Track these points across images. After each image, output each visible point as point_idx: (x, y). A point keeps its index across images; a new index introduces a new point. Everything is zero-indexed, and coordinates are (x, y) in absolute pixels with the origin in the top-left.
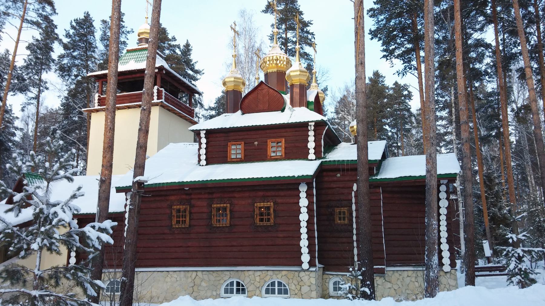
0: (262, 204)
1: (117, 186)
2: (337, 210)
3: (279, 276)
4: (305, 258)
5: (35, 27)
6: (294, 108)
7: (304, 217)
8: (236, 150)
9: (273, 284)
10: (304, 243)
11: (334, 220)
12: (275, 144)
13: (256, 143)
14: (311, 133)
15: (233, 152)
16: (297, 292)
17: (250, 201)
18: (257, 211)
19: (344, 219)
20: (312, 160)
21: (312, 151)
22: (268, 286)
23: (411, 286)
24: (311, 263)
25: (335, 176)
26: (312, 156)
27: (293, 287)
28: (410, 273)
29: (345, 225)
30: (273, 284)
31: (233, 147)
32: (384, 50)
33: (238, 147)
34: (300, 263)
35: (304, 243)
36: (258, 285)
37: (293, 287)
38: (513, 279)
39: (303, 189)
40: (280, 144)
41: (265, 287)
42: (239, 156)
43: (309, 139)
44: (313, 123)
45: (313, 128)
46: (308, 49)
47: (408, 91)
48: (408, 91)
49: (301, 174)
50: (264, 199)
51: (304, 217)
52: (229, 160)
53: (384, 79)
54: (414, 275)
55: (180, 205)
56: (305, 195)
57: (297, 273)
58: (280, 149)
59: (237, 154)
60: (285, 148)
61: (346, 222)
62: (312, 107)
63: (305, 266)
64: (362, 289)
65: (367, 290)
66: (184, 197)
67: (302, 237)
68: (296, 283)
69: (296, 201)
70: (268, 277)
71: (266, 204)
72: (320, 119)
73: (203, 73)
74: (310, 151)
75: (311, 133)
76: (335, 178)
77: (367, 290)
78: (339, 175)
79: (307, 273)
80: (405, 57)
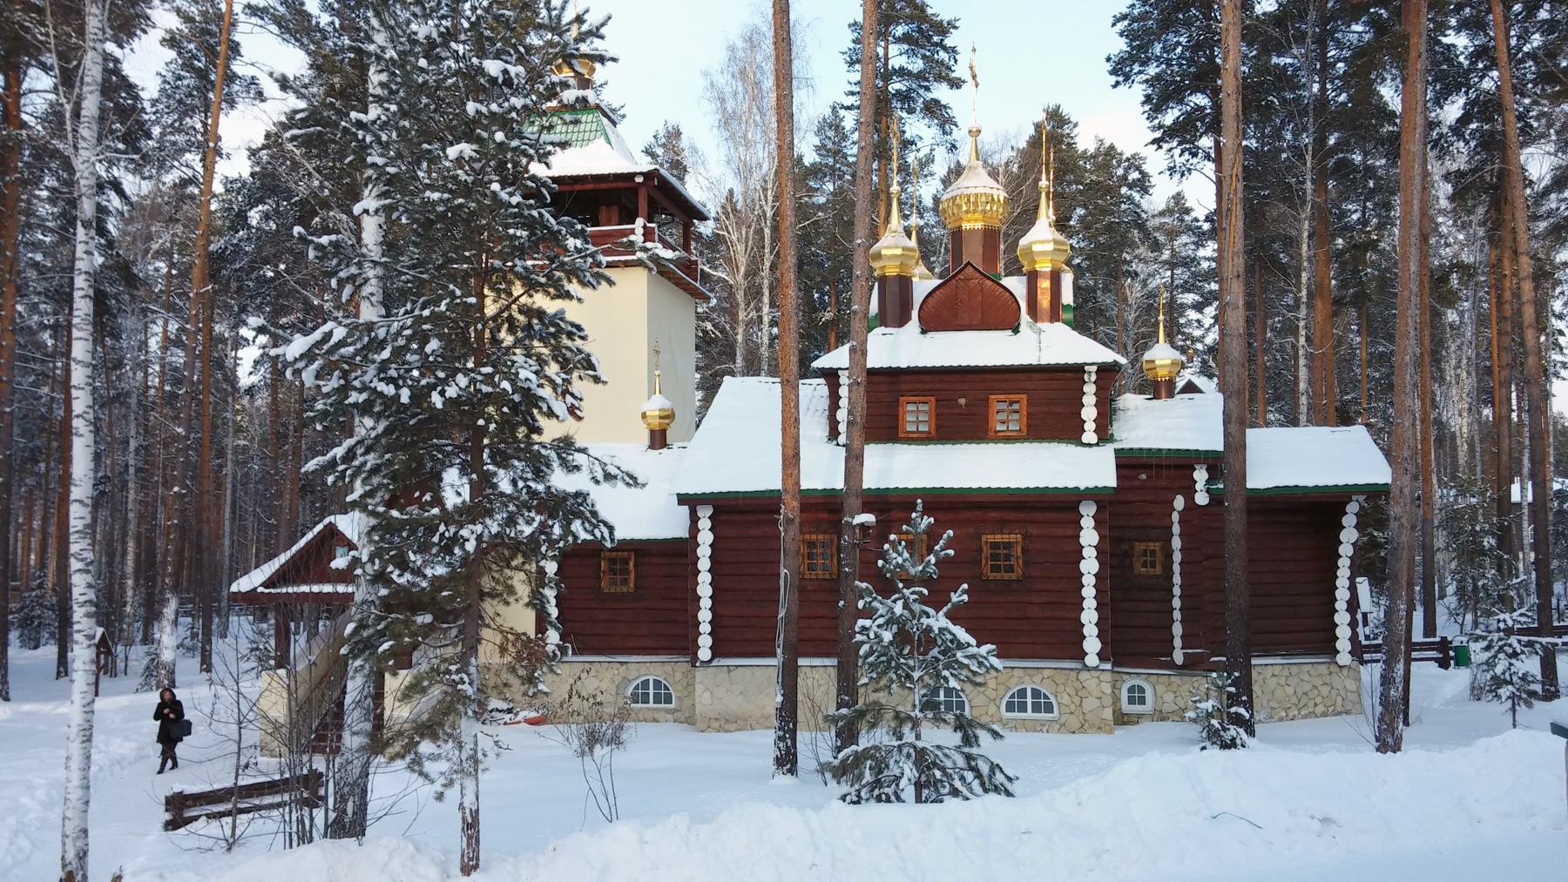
0: (998, 538)
1: (683, 492)
2: (1140, 547)
3: (1037, 678)
4: (1092, 645)
5: (274, 28)
6: (1039, 325)
7: (1089, 566)
8: (916, 415)
9: (1022, 693)
10: (1089, 616)
11: (1131, 567)
12: (1003, 406)
13: (962, 401)
14: (1090, 389)
15: (909, 418)
16: (1073, 708)
17: (971, 530)
18: (987, 551)
19: (1153, 565)
20: (1089, 445)
21: (1090, 426)
22: (1012, 696)
23: (1279, 694)
24: (1102, 656)
25: (1136, 478)
26: (1089, 436)
27: (1066, 699)
28: (1277, 670)
29: (1157, 577)
30: (1022, 693)
31: (910, 407)
32: (1154, 129)
33: (923, 407)
34: (1082, 655)
35: (1089, 616)
36: (993, 695)
37: (1066, 699)
38: (1501, 691)
39: (1088, 511)
40: (1016, 407)
41: (1006, 699)
42: (924, 428)
43: (1085, 400)
44: (1094, 368)
45: (1094, 377)
46: (940, 92)
47: (1141, 172)
48: (1141, 172)
49: (1091, 485)
50: (1001, 525)
51: (1089, 566)
52: (901, 435)
53: (1076, 131)
54: (1286, 672)
55: (818, 532)
56: (1092, 523)
57: (1073, 674)
58: (1016, 416)
59: (918, 422)
60: (1029, 415)
61: (1158, 570)
62: (1069, 316)
63: (1092, 660)
64: (1233, 710)
65: (1242, 711)
66: (825, 515)
67: (1085, 604)
68: (1072, 693)
69: (1070, 532)
70: (1015, 680)
71: (1005, 538)
72: (1110, 360)
73: (624, 116)
74: (1086, 426)
75: (1090, 389)
76: (1136, 483)
77: (1242, 711)
78: (1144, 476)
79: (1094, 673)
80: (1161, 96)
